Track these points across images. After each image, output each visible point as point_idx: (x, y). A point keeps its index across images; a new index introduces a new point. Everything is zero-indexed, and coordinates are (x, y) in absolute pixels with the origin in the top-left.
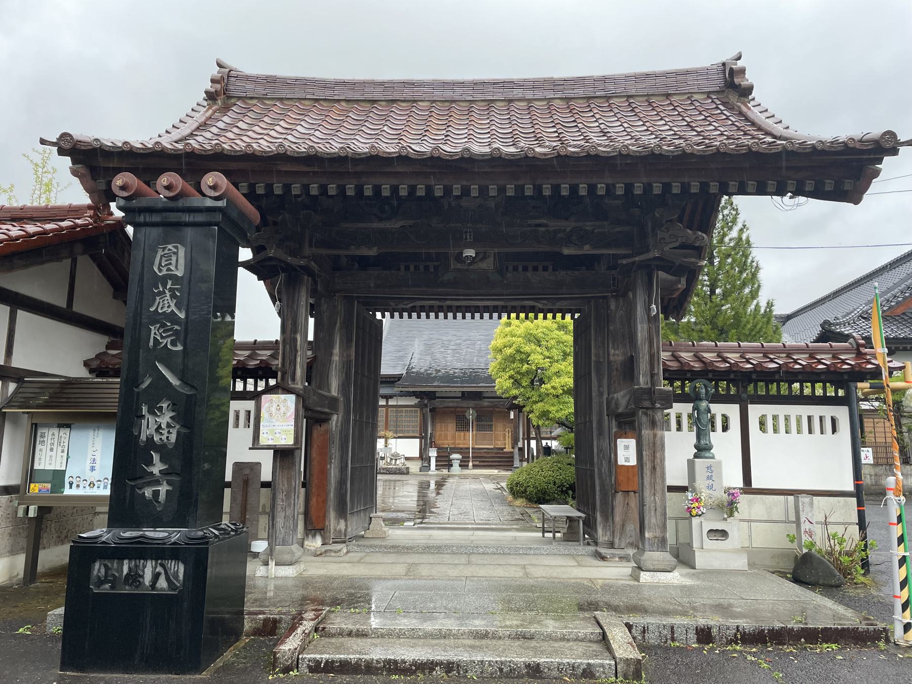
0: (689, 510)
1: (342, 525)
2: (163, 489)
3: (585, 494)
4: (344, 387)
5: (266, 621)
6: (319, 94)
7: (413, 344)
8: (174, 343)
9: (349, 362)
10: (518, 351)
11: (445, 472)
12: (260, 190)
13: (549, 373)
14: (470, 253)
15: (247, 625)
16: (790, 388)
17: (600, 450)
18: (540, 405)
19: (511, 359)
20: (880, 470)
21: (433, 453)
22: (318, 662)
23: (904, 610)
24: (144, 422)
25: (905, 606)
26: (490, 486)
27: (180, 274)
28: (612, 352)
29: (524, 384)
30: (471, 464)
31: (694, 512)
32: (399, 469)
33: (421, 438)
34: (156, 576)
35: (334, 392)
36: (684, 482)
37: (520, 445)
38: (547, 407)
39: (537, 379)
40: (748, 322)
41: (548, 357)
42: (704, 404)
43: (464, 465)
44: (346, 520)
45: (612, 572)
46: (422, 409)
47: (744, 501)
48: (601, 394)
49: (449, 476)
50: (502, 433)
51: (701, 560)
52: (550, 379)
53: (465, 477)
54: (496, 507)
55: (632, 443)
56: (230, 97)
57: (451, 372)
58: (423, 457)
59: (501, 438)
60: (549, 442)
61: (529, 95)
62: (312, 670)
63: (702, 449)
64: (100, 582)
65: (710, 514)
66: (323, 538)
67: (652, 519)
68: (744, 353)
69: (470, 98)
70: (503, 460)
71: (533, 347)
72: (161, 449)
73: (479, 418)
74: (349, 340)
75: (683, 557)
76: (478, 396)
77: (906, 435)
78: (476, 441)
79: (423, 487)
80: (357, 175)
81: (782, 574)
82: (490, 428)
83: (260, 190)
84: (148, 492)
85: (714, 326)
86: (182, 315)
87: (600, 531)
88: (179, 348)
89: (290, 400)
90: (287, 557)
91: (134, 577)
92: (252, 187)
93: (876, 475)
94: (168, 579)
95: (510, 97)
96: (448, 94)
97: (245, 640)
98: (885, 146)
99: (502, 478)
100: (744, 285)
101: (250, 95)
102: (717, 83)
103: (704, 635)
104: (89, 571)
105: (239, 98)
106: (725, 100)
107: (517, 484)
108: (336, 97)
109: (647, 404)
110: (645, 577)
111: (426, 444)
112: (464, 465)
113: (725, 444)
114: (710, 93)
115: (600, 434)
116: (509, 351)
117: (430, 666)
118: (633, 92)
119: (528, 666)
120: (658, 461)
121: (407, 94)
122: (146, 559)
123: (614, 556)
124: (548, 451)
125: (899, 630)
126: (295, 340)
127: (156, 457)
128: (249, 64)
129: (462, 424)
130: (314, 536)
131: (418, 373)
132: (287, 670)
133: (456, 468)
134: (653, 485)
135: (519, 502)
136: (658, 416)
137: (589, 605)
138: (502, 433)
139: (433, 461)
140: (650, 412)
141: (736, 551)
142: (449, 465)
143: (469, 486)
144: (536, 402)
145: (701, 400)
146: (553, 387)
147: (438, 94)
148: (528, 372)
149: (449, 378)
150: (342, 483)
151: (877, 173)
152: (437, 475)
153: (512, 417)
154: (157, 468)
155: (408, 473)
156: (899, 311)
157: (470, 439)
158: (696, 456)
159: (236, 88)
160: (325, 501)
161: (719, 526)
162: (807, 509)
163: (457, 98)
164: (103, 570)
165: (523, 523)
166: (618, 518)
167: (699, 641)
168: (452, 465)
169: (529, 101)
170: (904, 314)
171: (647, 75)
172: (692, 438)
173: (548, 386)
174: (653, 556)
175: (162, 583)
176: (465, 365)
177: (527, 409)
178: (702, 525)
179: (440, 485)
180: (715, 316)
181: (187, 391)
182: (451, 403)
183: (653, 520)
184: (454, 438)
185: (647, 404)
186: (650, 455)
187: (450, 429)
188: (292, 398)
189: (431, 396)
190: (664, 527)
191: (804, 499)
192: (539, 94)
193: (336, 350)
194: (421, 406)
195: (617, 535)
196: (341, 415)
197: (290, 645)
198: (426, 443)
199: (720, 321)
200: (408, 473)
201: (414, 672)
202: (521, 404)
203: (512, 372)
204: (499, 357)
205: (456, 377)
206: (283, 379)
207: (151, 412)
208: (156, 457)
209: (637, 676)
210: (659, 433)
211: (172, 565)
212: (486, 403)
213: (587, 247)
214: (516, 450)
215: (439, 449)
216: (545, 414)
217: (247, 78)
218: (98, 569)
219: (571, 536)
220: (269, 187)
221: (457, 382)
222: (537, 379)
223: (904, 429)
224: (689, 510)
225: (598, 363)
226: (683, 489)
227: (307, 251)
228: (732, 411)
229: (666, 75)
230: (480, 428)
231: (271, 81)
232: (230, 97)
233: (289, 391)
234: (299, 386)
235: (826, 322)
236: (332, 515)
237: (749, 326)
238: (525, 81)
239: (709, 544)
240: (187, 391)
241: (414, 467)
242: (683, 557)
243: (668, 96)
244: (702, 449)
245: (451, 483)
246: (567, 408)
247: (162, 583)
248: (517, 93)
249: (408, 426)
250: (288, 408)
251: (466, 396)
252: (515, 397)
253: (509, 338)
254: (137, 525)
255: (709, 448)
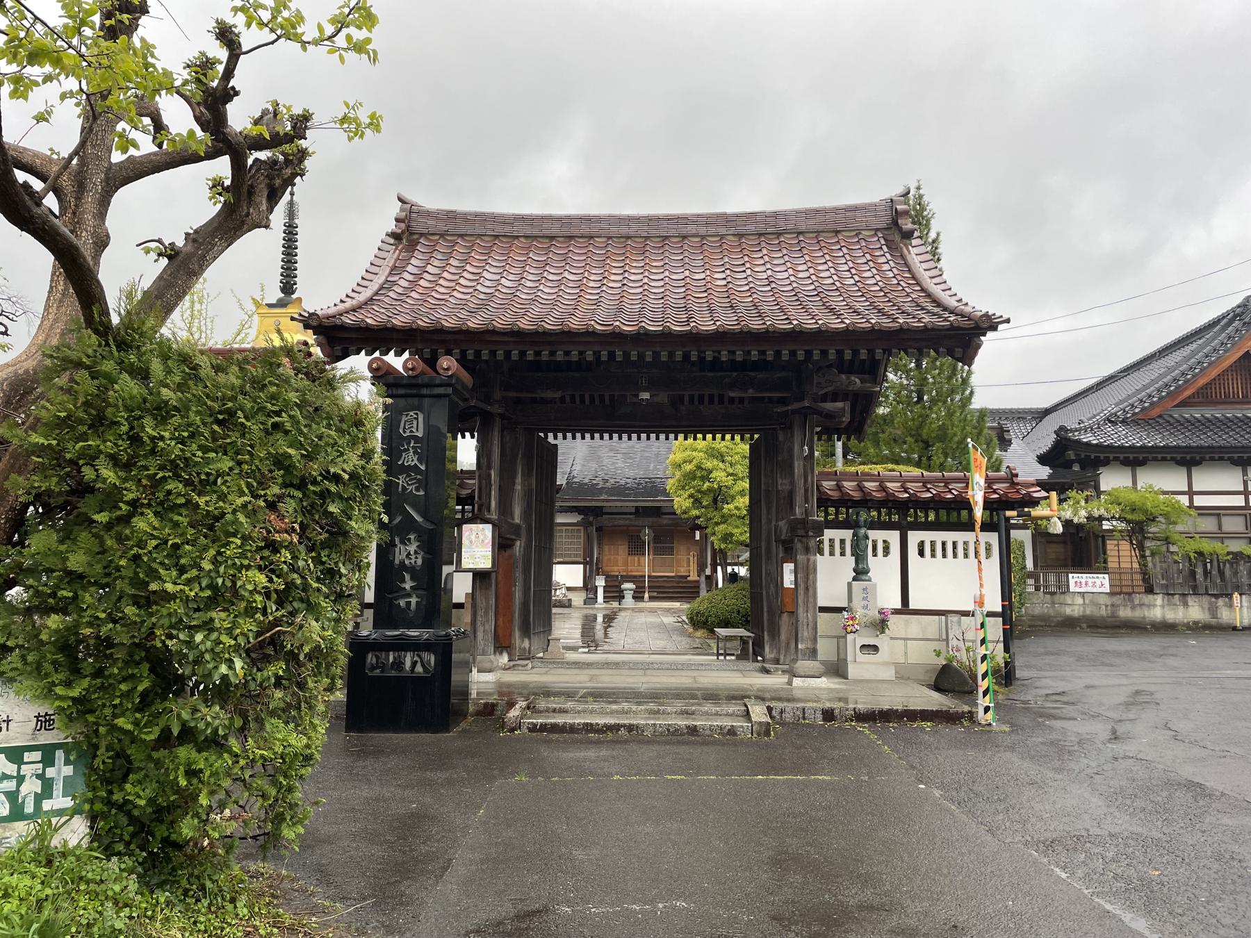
0: (845, 627)
1: (526, 644)
2: (414, 600)
3: (760, 620)
4: (526, 514)
5: (486, 705)
6: (499, 230)
7: (582, 458)
8: (417, 490)
9: (530, 491)
10: (699, 467)
11: (615, 604)
12: (470, 355)
13: (732, 492)
14: (645, 396)
15: (471, 708)
16: (959, 514)
17: (768, 574)
18: (722, 527)
19: (691, 476)
20: (1117, 600)
21: (600, 582)
22: (535, 725)
23: (984, 696)
24: (397, 550)
25: (985, 693)
26: (669, 620)
27: (420, 434)
28: (780, 481)
29: (705, 503)
30: (646, 595)
31: (849, 629)
32: (560, 601)
33: (585, 564)
34: (414, 664)
35: (517, 520)
36: (844, 605)
37: (708, 572)
38: (730, 529)
39: (718, 497)
40: (955, 435)
41: (732, 475)
42: (863, 531)
43: (638, 597)
44: (530, 639)
45: (775, 681)
46: (586, 529)
47: (893, 621)
48: (769, 522)
49: (620, 610)
50: (685, 558)
51: (853, 671)
52: (733, 498)
53: (641, 610)
54: (674, 637)
55: (792, 566)
56: (412, 234)
57: (623, 482)
58: (589, 586)
59: (685, 565)
60: (736, 568)
61: (702, 231)
62: (530, 730)
63: (861, 572)
64: (373, 668)
65: (864, 631)
66: (510, 655)
67: (805, 633)
68: (905, 482)
69: (645, 234)
70: (681, 590)
71: (715, 462)
72: (412, 570)
73: (657, 539)
74: (530, 470)
75: (837, 669)
76: (657, 512)
77: (1149, 559)
78: (653, 567)
79: (589, 623)
80: (550, 343)
81: (929, 686)
82: (670, 551)
83: (470, 355)
84: (402, 603)
85: (918, 438)
86: (423, 468)
87: (767, 649)
88: (422, 493)
89: (488, 529)
90: (488, 665)
91: (399, 664)
92: (463, 353)
93: (1113, 605)
94: (423, 665)
95: (684, 232)
96: (624, 231)
97: (470, 719)
98: (989, 324)
99: (680, 610)
100: (953, 392)
101: (431, 230)
102: (884, 220)
103: (828, 715)
104: (365, 658)
105: (422, 235)
106: (889, 238)
107: (698, 613)
108: (515, 234)
109: (801, 532)
110: (797, 682)
111: (591, 571)
112: (638, 597)
113: (884, 570)
114: (877, 230)
115: (769, 558)
116: (689, 467)
117: (617, 727)
118: (803, 228)
119: (688, 727)
120: (810, 582)
121: (585, 230)
122: (406, 651)
123: (777, 670)
124: (734, 577)
125: (981, 711)
126: (490, 475)
127: (407, 577)
128: (430, 200)
129: (636, 547)
130: (501, 653)
131: (581, 485)
132: (512, 730)
133: (628, 601)
134: (806, 603)
135: (699, 633)
136: (812, 543)
137: (738, 696)
138: (685, 558)
139: (600, 592)
140: (804, 540)
141: (886, 664)
142: (620, 597)
143: (642, 619)
144: (717, 524)
145: (860, 527)
146: (737, 508)
147: (614, 230)
148: (710, 490)
149: (619, 490)
150: (525, 605)
151: (979, 346)
152: (606, 609)
153: (698, 537)
154: (408, 585)
155: (570, 606)
156: (1155, 412)
157: (646, 565)
158: (854, 579)
159: (418, 227)
160: (511, 621)
161: (871, 641)
162: (955, 627)
163: (632, 234)
164: (374, 660)
165: (701, 650)
166: (783, 637)
167: (824, 719)
168: (623, 597)
169: (703, 237)
170: (1160, 416)
171: (817, 211)
172: (850, 561)
173: (731, 506)
174: (804, 665)
175: (419, 669)
176: (641, 474)
177: (709, 531)
178: (854, 642)
179: (609, 619)
180: (921, 426)
181: (428, 526)
182: (621, 521)
183: (806, 634)
184: (626, 564)
185: (801, 532)
186: (807, 576)
187: (621, 552)
188: (489, 526)
189: (598, 512)
190: (815, 640)
191: (954, 619)
192: (712, 230)
193: (519, 480)
194: (585, 524)
195: (783, 652)
196: (524, 540)
197: (514, 713)
198: (592, 569)
199: (925, 433)
200: (570, 606)
201: (605, 732)
202: (703, 524)
203: (692, 491)
204: (678, 474)
205: (628, 489)
206: (480, 509)
207: (403, 542)
208: (407, 577)
209: (767, 733)
210: (812, 558)
211: (425, 655)
212: (665, 520)
213: (751, 391)
214: (703, 578)
215: (608, 578)
216: (727, 537)
217: (428, 214)
218: (371, 658)
219: (743, 656)
220: (478, 354)
221: (628, 495)
222: (718, 497)
223: (1148, 553)
224: (845, 627)
225: (767, 491)
226: (838, 610)
227: (498, 395)
228: (894, 537)
229: (836, 210)
230: (658, 551)
231: (451, 216)
232: (412, 234)
233: (486, 521)
234: (494, 516)
235: (1062, 428)
236: (517, 634)
237: (956, 439)
238: (698, 216)
239: (861, 657)
240: (428, 526)
241: (578, 599)
242: (837, 669)
243: (837, 232)
244: (861, 572)
245: (622, 618)
246: (742, 533)
247: (419, 669)
248: (691, 229)
249: (569, 549)
250: (485, 536)
251: (640, 512)
252: (698, 517)
253: (688, 453)
254: (396, 628)
255: (866, 572)
